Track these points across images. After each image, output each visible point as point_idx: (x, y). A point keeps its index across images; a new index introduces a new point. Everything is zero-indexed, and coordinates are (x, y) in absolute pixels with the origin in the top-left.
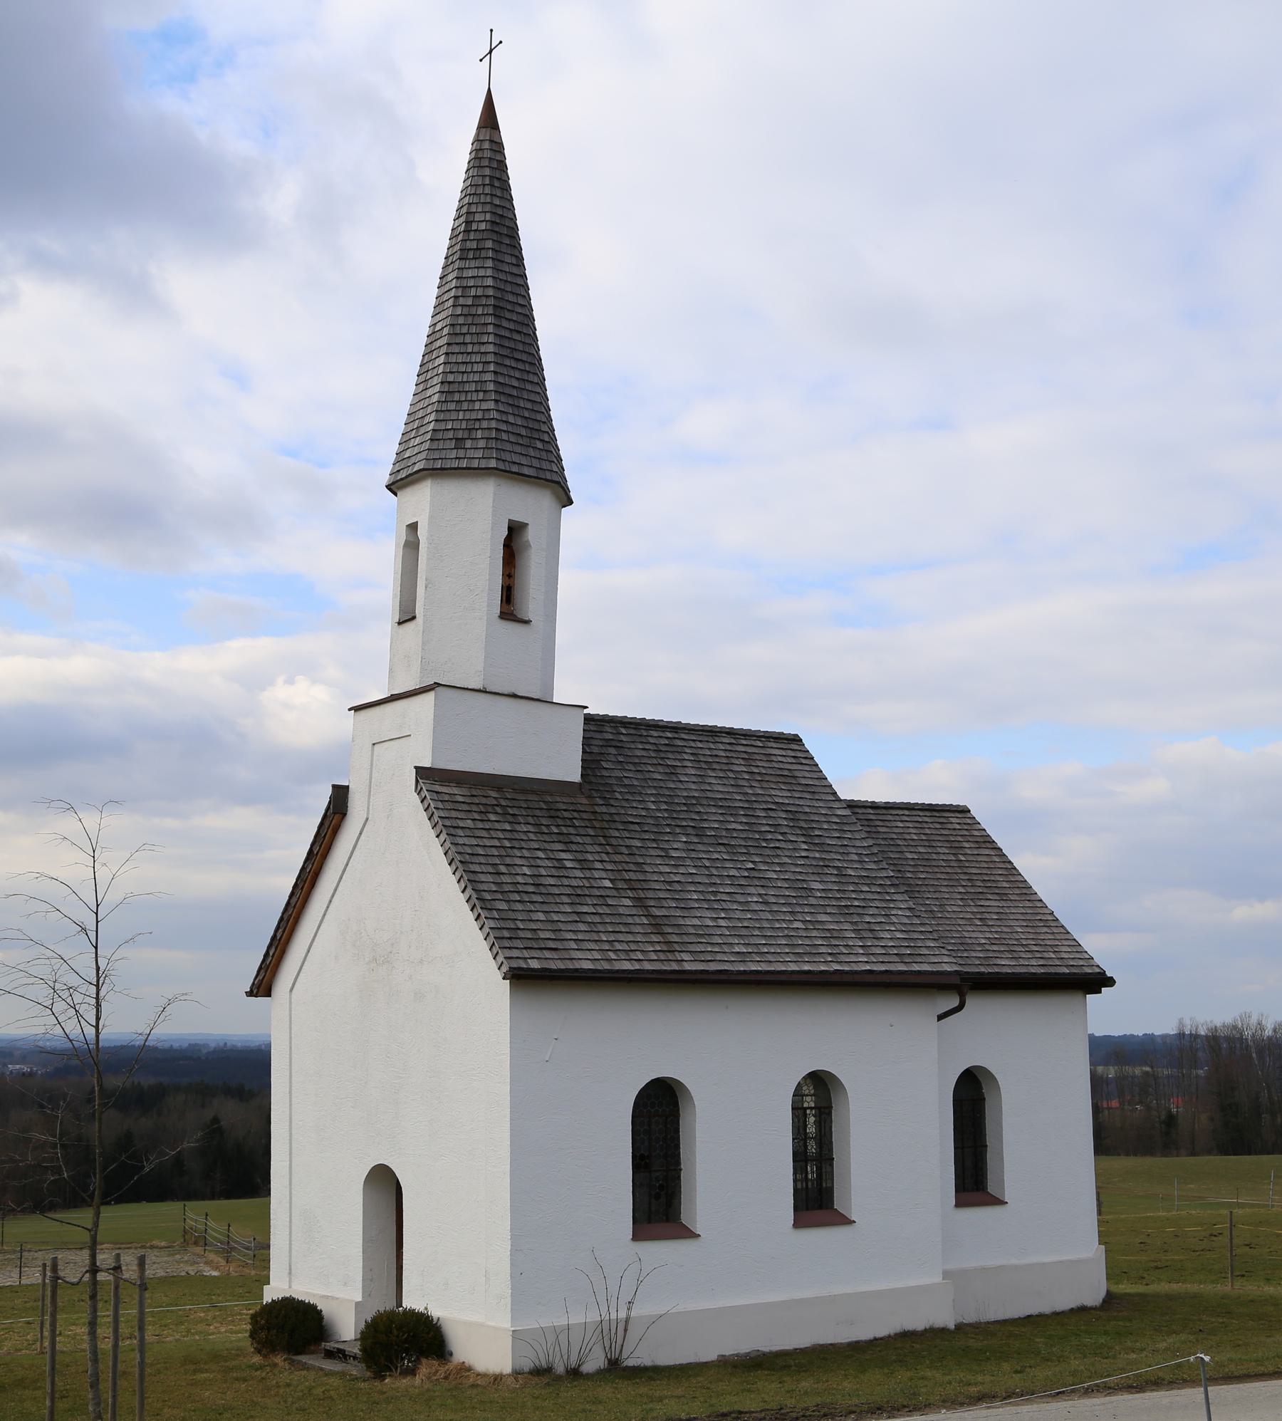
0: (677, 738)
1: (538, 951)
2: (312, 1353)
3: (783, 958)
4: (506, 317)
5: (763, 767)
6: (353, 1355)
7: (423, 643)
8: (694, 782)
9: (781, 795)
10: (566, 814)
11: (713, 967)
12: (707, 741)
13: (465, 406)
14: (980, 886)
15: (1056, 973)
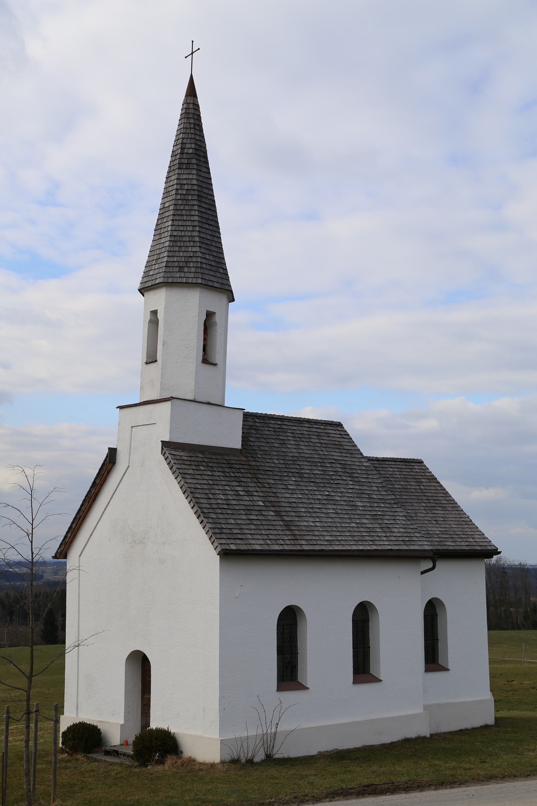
0: (283, 424)
1: (234, 540)
2: (96, 752)
3: (349, 543)
4: (204, 201)
5: (326, 440)
6: (123, 753)
7: (162, 375)
8: (294, 448)
9: (336, 455)
10: (237, 466)
11: (317, 548)
12: (298, 426)
13: (183, 249)
14: (432, 503)
15: (474, 550)
